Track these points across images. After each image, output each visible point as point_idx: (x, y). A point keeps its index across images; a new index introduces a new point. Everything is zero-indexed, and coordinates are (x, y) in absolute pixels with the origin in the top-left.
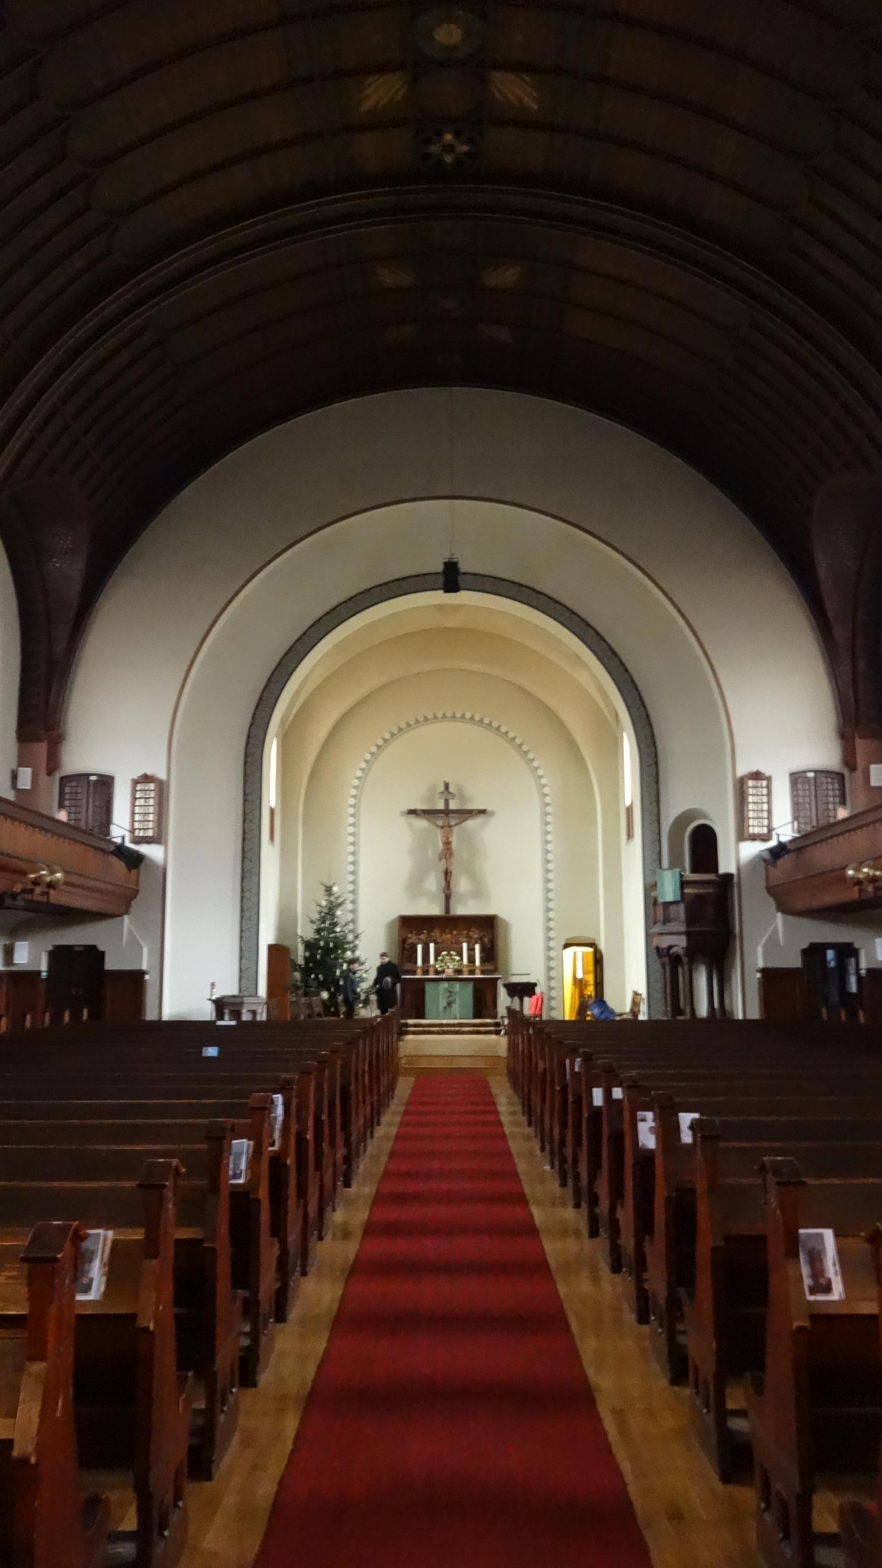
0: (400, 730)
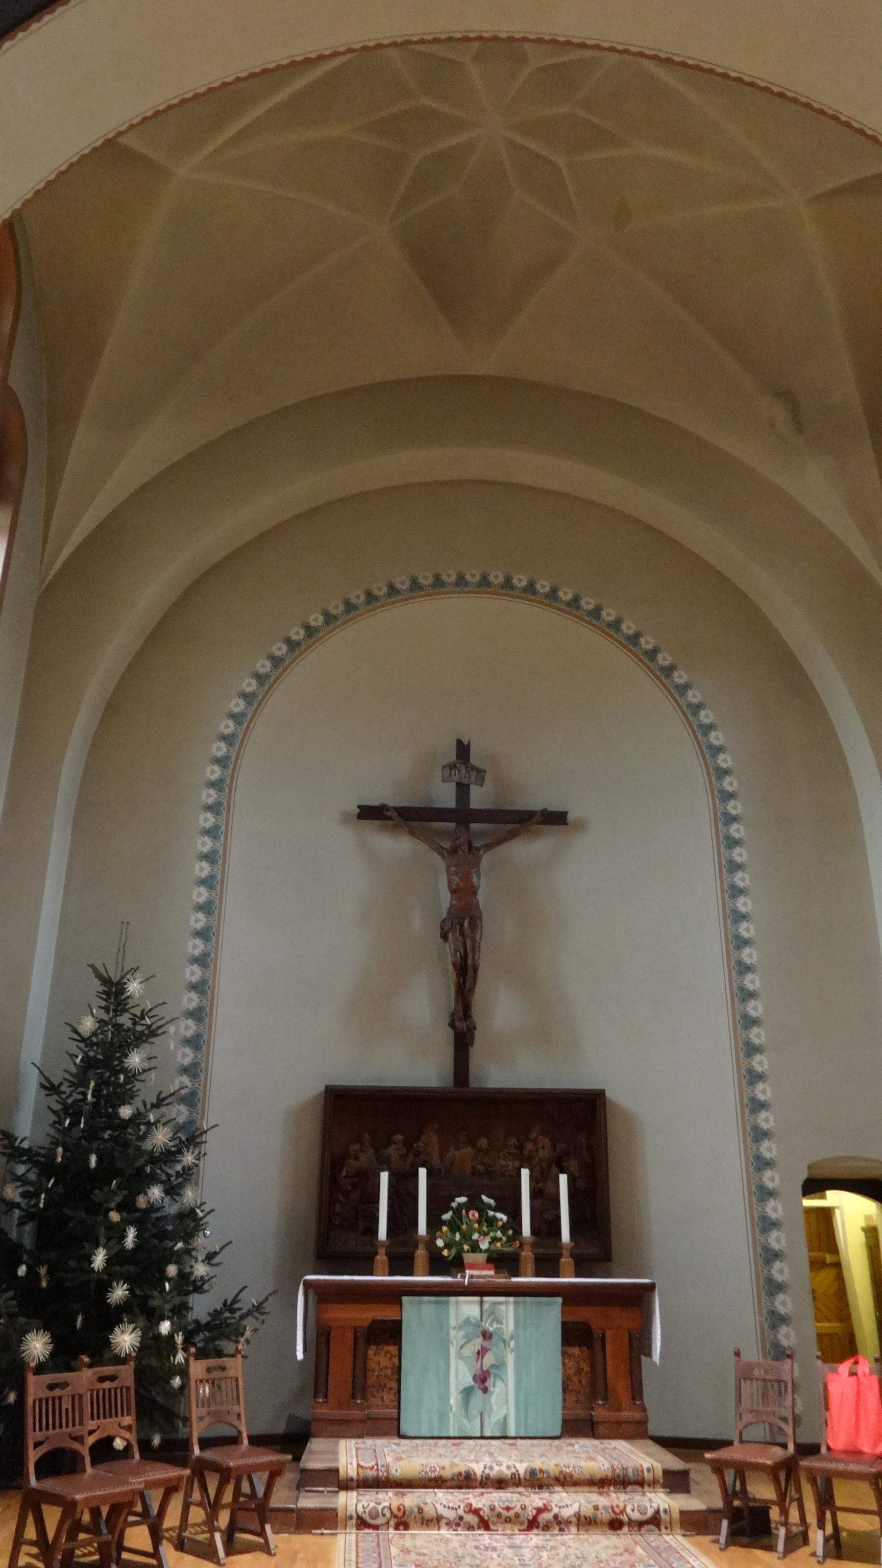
0: (350, 607)
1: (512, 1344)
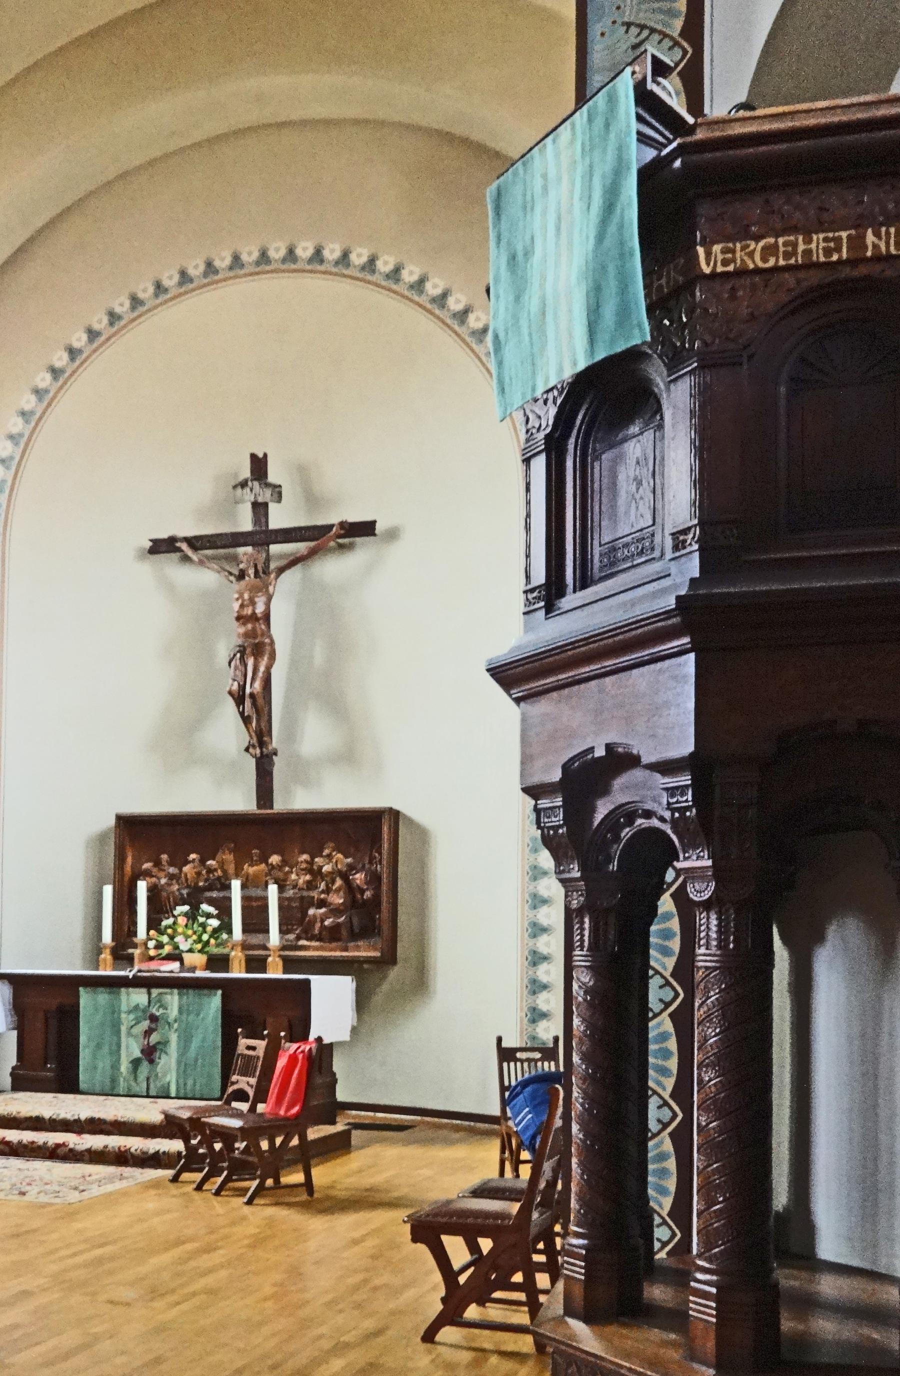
1: (176, 1025)
